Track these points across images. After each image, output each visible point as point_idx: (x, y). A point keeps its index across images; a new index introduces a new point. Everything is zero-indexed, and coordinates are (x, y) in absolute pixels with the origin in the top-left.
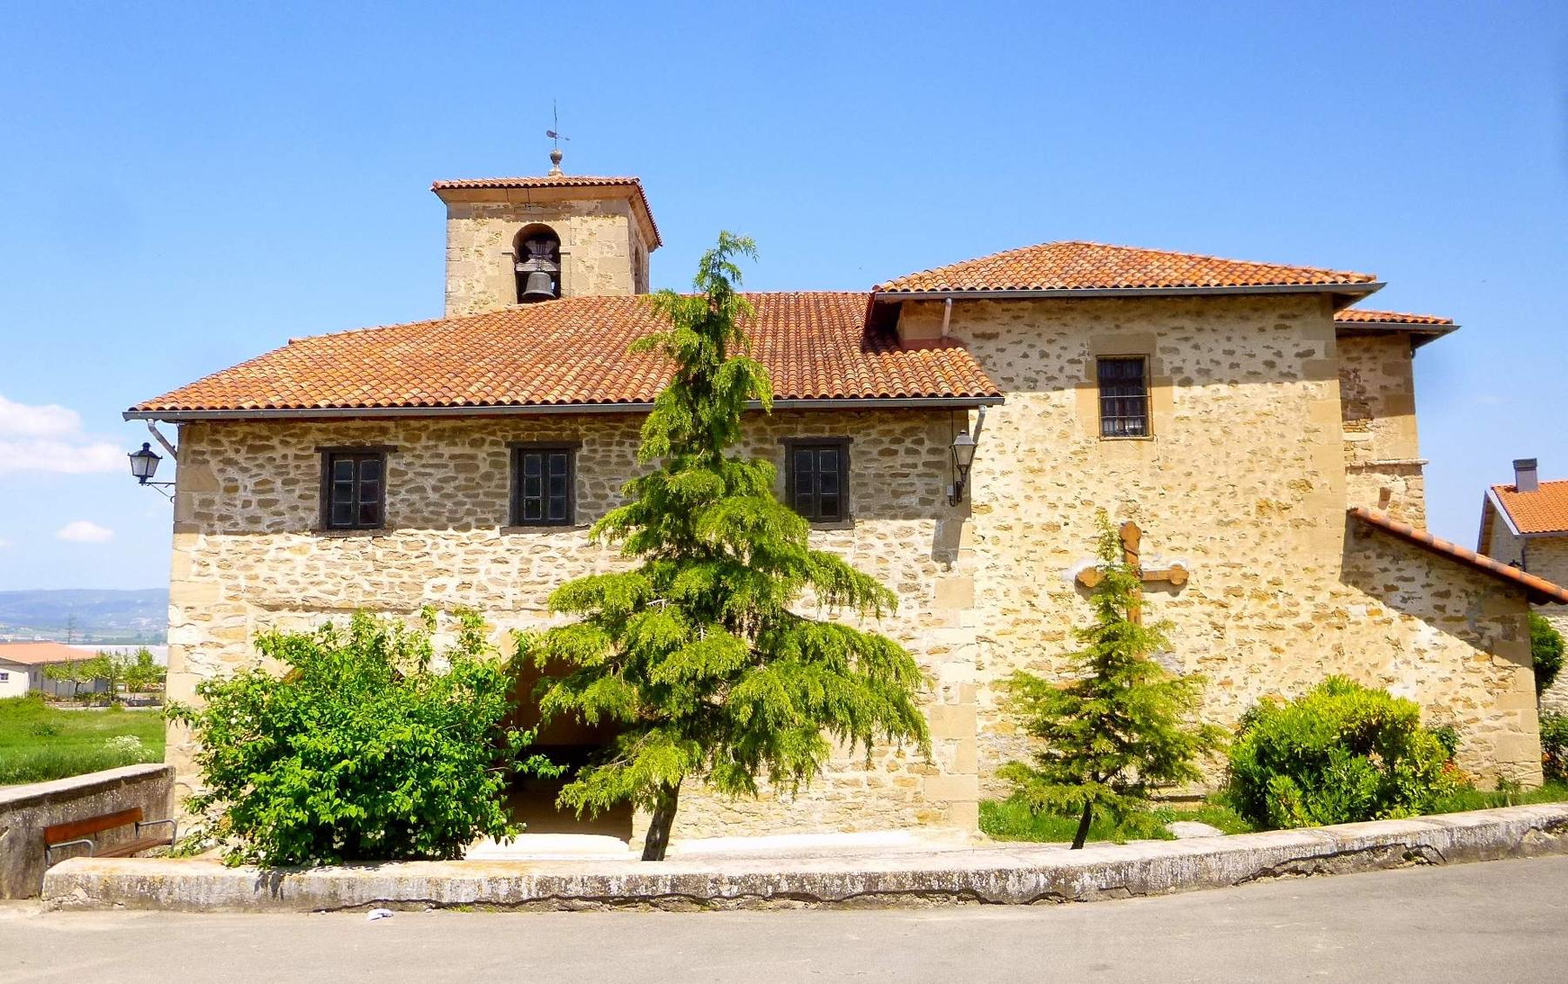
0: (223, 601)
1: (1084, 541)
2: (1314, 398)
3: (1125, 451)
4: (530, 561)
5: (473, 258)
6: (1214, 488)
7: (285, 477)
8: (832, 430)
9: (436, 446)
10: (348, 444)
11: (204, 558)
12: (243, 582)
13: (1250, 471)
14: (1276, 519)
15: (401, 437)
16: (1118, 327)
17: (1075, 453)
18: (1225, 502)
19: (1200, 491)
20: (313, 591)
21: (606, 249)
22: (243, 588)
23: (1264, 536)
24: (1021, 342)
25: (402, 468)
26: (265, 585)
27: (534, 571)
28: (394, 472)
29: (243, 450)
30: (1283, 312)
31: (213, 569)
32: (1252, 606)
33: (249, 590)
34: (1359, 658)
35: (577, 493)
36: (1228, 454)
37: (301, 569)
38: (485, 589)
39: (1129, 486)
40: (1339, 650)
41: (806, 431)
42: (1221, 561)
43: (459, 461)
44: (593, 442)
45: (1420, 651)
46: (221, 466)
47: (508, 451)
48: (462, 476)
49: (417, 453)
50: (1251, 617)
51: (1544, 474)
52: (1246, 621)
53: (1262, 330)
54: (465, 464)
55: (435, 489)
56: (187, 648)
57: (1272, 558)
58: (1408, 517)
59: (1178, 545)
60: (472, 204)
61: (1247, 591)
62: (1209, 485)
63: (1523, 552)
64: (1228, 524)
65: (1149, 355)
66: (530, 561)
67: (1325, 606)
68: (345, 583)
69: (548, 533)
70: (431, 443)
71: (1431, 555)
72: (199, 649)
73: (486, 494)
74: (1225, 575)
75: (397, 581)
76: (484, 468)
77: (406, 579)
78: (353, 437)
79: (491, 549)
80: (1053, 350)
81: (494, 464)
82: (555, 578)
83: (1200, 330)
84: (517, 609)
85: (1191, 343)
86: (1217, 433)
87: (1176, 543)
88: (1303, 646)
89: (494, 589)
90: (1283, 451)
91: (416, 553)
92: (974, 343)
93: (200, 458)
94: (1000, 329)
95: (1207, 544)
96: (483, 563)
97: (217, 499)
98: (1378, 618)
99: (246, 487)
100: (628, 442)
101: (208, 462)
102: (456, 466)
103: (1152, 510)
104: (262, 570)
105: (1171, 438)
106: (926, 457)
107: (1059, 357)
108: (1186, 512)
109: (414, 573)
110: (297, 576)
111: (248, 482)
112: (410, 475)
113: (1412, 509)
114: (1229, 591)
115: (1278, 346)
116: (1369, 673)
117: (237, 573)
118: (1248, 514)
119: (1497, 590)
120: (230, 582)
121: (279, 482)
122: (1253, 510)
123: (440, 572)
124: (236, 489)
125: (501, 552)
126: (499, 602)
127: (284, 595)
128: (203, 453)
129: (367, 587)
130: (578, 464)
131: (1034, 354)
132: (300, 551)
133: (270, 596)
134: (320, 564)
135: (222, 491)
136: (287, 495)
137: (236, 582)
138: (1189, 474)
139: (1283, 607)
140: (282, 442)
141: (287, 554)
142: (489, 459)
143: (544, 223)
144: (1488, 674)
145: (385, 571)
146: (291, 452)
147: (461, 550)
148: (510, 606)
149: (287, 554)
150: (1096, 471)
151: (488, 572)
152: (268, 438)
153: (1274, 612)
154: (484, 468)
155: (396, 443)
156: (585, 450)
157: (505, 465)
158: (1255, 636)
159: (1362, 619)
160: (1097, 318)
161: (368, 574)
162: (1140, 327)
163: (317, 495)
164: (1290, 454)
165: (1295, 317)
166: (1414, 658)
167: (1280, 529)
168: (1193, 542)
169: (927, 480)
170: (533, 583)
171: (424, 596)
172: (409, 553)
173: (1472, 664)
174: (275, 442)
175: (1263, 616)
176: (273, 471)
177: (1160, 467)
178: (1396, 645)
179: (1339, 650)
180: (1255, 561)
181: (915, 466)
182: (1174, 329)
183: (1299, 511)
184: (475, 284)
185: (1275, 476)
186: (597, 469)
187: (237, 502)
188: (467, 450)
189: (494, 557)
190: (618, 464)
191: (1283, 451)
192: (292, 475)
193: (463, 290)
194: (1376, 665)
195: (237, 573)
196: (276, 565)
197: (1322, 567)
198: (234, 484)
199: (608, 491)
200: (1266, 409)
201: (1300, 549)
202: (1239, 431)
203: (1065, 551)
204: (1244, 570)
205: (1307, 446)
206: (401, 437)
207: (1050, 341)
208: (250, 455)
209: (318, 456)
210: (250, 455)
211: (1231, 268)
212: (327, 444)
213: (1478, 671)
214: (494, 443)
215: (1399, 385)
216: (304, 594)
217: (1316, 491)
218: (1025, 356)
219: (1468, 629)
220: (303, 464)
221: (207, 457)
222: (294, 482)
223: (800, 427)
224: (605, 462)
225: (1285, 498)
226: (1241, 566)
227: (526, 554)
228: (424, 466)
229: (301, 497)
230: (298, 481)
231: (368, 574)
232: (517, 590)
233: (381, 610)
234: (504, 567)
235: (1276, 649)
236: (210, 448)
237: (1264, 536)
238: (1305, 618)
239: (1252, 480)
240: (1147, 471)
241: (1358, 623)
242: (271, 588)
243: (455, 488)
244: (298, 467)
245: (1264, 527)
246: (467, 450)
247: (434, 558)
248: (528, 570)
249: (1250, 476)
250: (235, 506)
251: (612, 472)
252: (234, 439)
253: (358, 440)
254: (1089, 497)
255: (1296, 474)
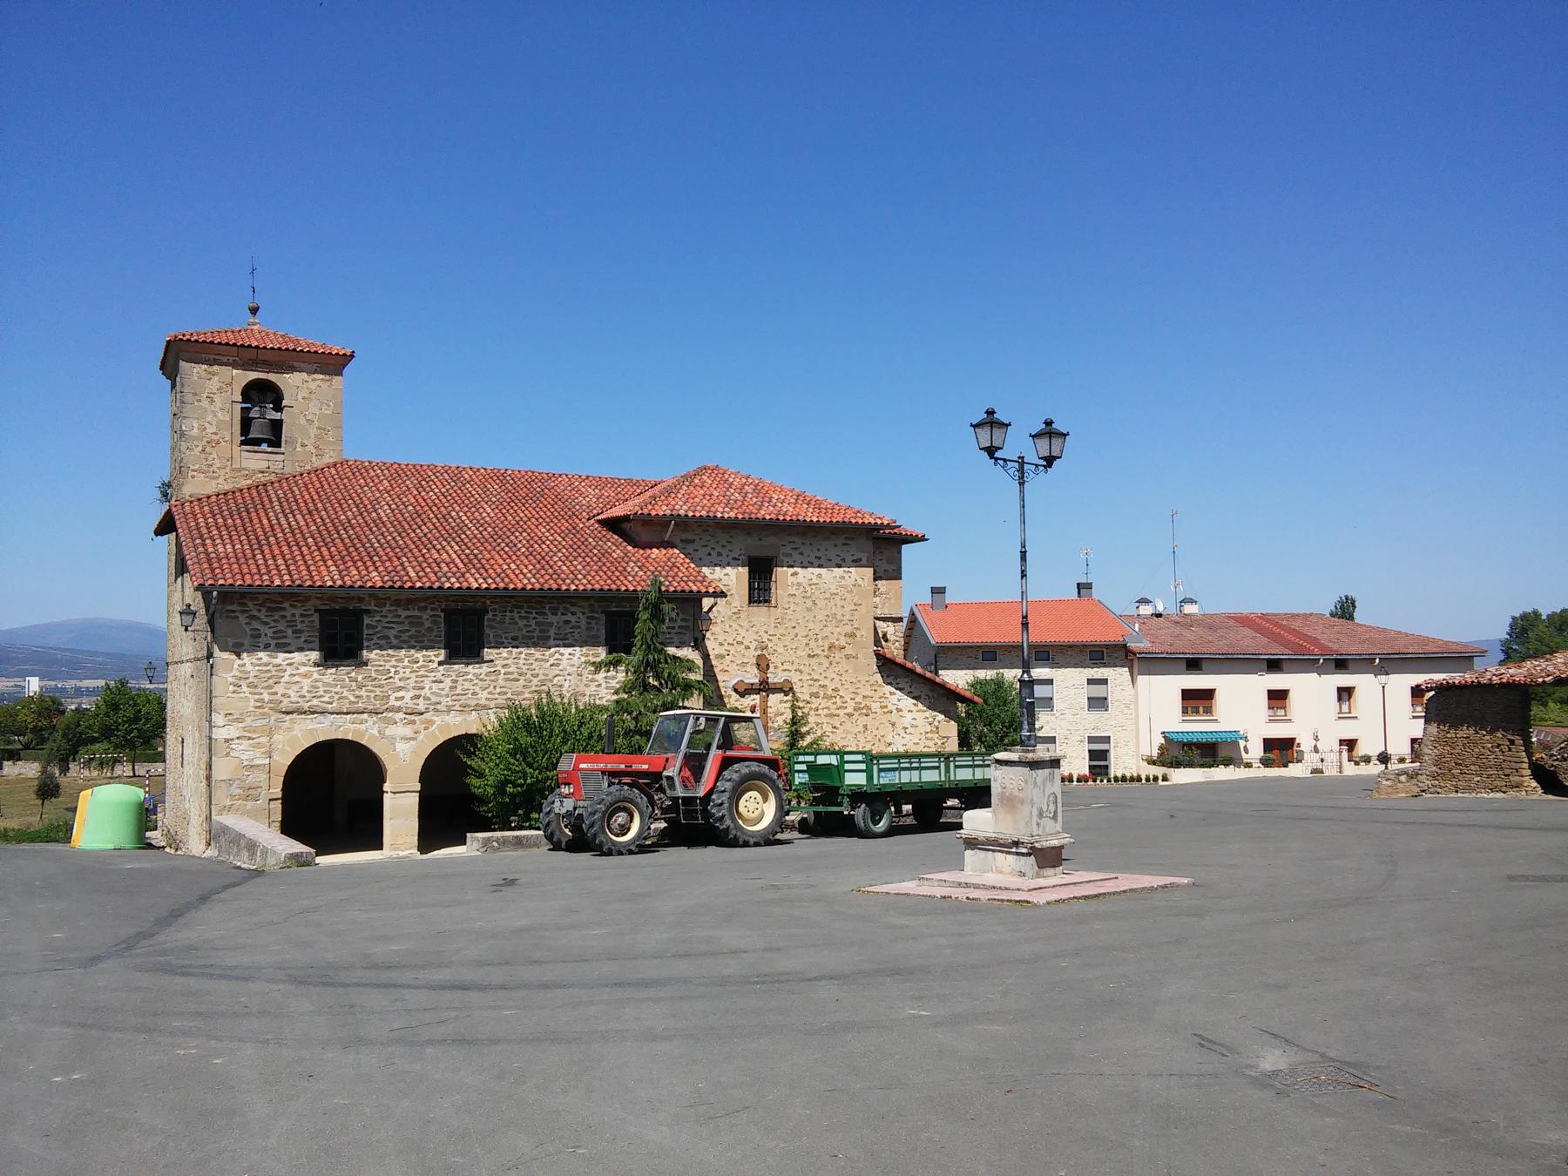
0: (252, 709)
1: (737, 665)
2: (860, 586)
3: (760, 612)
4: (457, 681)
5: (205, 403)
6: (806, 636)
7: (294, 628)
8: (631, 606)
9: (396, 610)
10: (337, 607)
11: (238, 681)
12: (266, 697)
13: (825, 626)
14: (838, 655)
15: (373, 604)
16: (760, 540)
17: (734, 613)
18: (813, 644)
19: (799, 637)
20: (315, 702)
21: (325, 407)
22: (266, 700)
23: (831, 663)
24: (706, 546)
25: (374, 624)
26: (282, 699)
27: (459, 688)
28: (369, 627)
29: (264, 610)
30: (847, 536)
31: (245, 688)
32: (825, 703)
33: (270, 701)
34: (875, 732)
35: (485, 640)
36: (815, 617)
37: (306, 688)
38: (429, 699)
39: (762, 633)
40: (865, 727)
41: (617, 607)
42: (809, 678)
43: (411, 619)
44: (495, 610)
45: (905, 728)
46: (247, 620)
47: (442, 614)
48: (414, 629)
49: (383, 614)
50: (823, 709)
51: (950, 598)
52: (820, 712)
53: (836, 545)
54: (415, 622)
55: (396, 637)
56: (227, 741)
57: (835, 676)
58: (895, 648)
59: (787, 668)
60: (204, 356)
61: (822, 694)
62: (806, 634)
63: (936, 655)
64: (813, 656)
65: (776, 557)
66: (457, 681)
67: (860, 703)
68: (337, 697)
69: (467, 664)
70: (393, 608)
71: (914, 676)
72: (237, 741)
73: (429, 640)
74: (810, 685)
75: (372, 695)
76: (427, 624)
77: (378, 693)
78: (341, 603)
79: (433, 674)
80: (724, 552)
81: (434, 622)
82: (472, 691)
83: (803, 544)
84: (449, 710)
85: (799, 551)
86: (809, 603)
87: (785, 667)
88: (848, 726)
89: (434, 699)
90: (843, 616)
91: (385, 677)
92: (681, 545)
93: (233, 615)
94: (696, 538)
95: (801, 667)
96: (427, 684)
97: (246, 642)
98: (886, 710)
99: (266, 635)
100: (516, 610)
101: (238, 617)
102: (409, 623)
103: (775, 648)
104: (280, 689)
105: (787, 606)
106: (680, 623)
107: (727, 556)
108: (792, 649)
109: (383, 689)
110: (304, 692)
111: (264, 629)
112: (379, 628)
113: (897, 643)
114: (812, 695)
115: (843, 555)
116: (879, 740)
117: (262, 691)
118: (823, 651)
119: (943, 695)
120: (257, 697)
121: (290, 631)
122: (826, 649)
123: (400, 689)
124: (259, 636)
125: (439, 675)
126: (438, 707)
127: (295, 705)
128: (234, 611)
129: (352, 699)
130: (486, 623)
131: (714, 553)
132: (305, 676)
133: (285, 704)
134: (320, 684)
135: (249, 637)
136: (295, 640)
137: (262, 697)
138: (794, 627)
139: (839, 703)
140: (291, 605)
141: (297, 679)
142: (431, 619)
143: (272, 377)
144: (937, 740)
145: (364, 688)
146: (297, 612)
147: (413, 675)
148: (445, 709)
149: (297, 679)
150: (745, 624)
151: (431, 688)
152: (281, 602)
153: (835, 706)
154: (427, 624)
155: (369, 608)
156: (490, 615)
157: (441, 623)
158: (825, 720)
159: (878, 710)
160: (749, 534)
161: (353, 690)
162: (773, 540)
163: (317, 640)
164: (847, 617)
165: (853, 539)
166: (902, 732)
167: (840, 660)
168: (795, 667)
169: (680, 636)
170: (458, 695)
171: (390, 704)
172: (380, 677)
173: (929, 735)
174: (286, 605)
175: (828, 708)
176: (286, 624)
177: (778, 624)
178: (893, 725)
179: (865, 727)
180: (826, 677)
181: (674, 628)
182: (790, 542)
183: (849, 650)
184: (207, 425)
185: (839, 629)
186: (497, 626)
187: (261, 645)
188: (416, 613)
189: (434, 679)
190: (509, 623)
191: (843, 616)
192: (298, 627)
193: (196, 430)
194: (883, 736)
195: (262, 691)
196: (290, 685)
197: (859, 681)
198: (258, 632)
199: (504, 640)
200: (835, 591)
201: (849, 671)
202: (821, 604)
203: (727, 671)
204: (820, 683)
205: (855, 613)
206: (373, 604)
207: (724, 546)
208: (269, 614)
209: (317, 614)
210: (269, 614)
211: (818, 505)
212: (323, 607)
213: (931, 739)
214: (432, 609)
215: (894, 570)
216: (309, 704)
217: (858, 638)
218: (709, 554)
219: (928, 716)
220: (306, 620)
221: (237, 614)
222: (301, 631)
223: (614, 604)
224: (502, 622)
225: (843, 643)
226: (818, 680)
227: (454, 678)
228: (388, 622)
229: (305, 641)
230: (303, 631)
231: (353, 690)
232: (449, 699)
233: (363, 713)
234: (441, 685)
235: (834, 727)
236: (239, 608)
237: (831, 663)
238: (850, 710)
239: (826, 632)
240: (773, 625)
241: (876, 713)
242: (286, 701)
243: (409, 636)
244: (302, 622)
245: (831, 658)
246: (416, 613)
247: (396, 680)
248: (456, 687)
249: (825, 629)
250: (259, 647)
251: (506, 628)
252: (256, 603)
253: (344, 605)
254: (741, 640)
255: (848, 629)
